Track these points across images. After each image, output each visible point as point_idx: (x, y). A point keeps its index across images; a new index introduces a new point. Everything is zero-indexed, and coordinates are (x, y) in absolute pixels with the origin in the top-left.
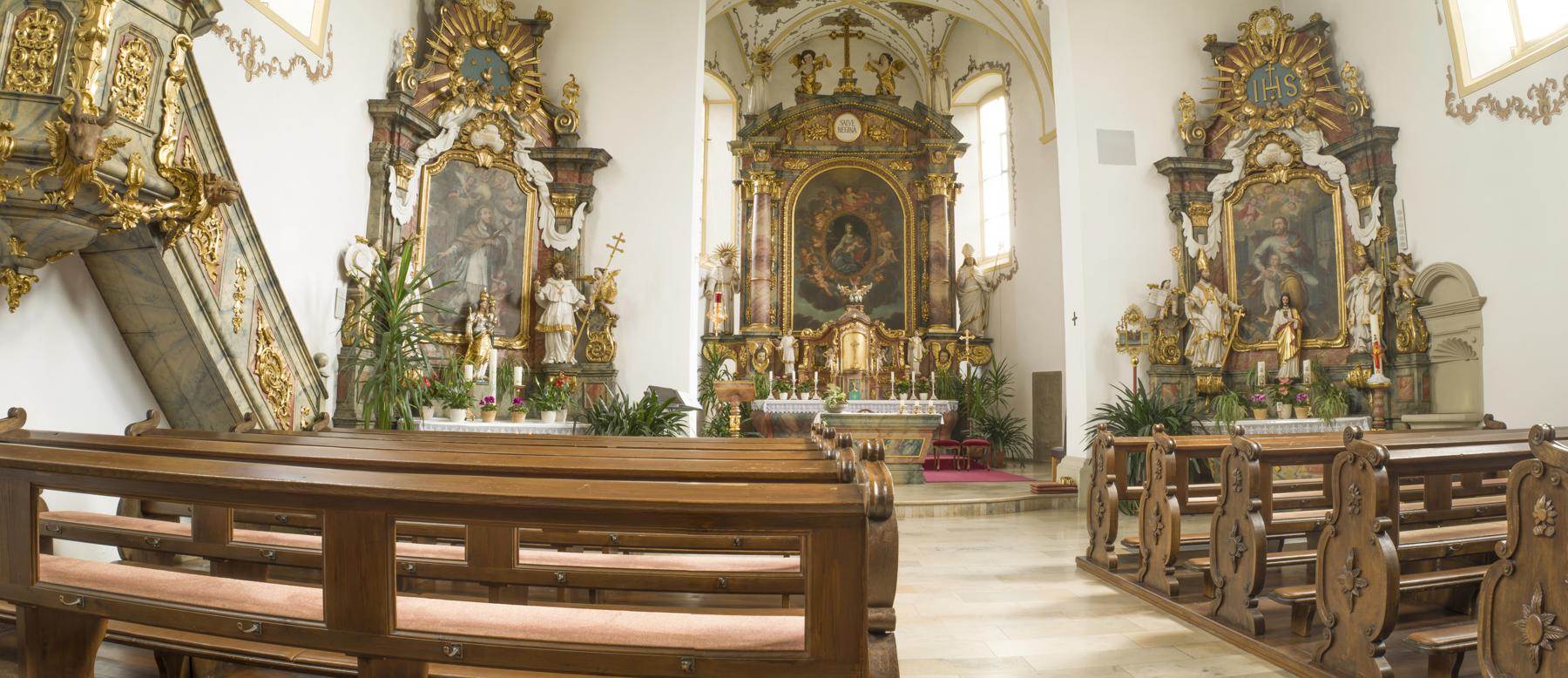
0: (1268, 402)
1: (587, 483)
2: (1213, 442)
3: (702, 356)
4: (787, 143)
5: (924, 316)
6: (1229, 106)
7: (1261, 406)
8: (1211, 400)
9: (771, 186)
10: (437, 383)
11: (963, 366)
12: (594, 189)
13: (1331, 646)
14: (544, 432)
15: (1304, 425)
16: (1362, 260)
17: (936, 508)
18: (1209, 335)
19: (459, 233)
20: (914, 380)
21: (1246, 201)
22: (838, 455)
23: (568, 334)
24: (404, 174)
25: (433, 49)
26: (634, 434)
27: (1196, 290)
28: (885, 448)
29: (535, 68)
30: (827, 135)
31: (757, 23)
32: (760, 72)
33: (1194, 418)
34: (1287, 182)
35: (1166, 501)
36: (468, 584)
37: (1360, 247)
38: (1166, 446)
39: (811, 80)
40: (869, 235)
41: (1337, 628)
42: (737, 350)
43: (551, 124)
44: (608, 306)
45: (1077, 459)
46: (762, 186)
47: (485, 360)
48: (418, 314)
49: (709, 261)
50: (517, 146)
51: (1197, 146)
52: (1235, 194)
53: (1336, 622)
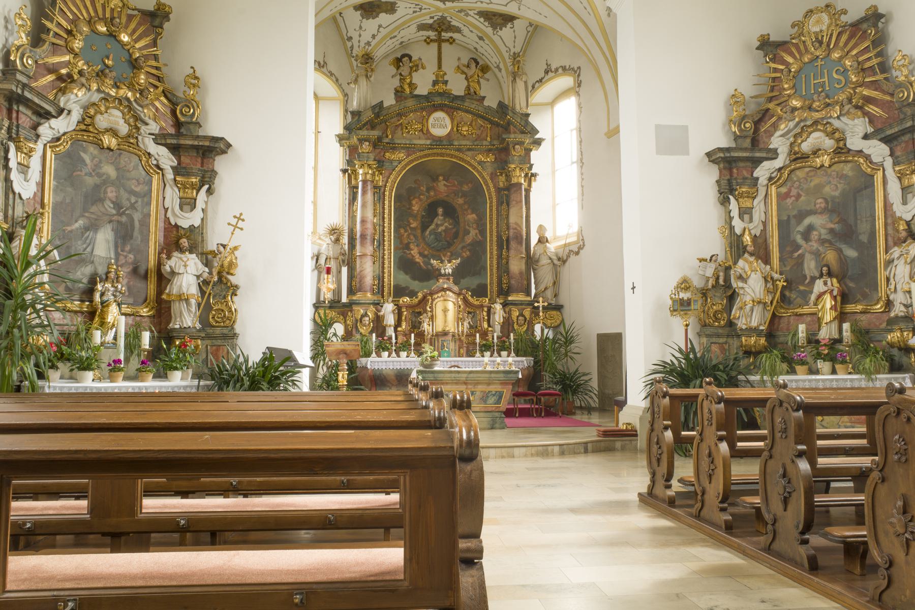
0: (809, 359)
1: (207, 435)
2: (758, 394)
3: (314, 320)
4: (387, 136)
5: (504, 286)
6: (777, 100)
7: (803, 363)
8: (755, 358)
9: (373, 175)
10: (64, 348)
11: (538, 328)
12: (216, 173)
13: (888, 586)
14: (170, 390)
15: (846, 380)
16: (904, 234)
17: (516, 450)
18: (753, 301)
19: (85, 210)
20: (495, 340)
21: (789, 184)
22: (431, 405)
23: (193, 301)
24: (25, 151)
25: (49, 30)
26: (254, 390)
27: (741, 263)
28: (471, 398)
29: (156, 58)
30: (422, 130)
31: (361, 27)
32: (364, 73)
33: (740, 373)
34: (830, 166)
35: (716, 445)
36: (91, 536)
37: (901, 222)
38: (715, 397)
39: (408, 81)
40: (458, 217)
41: (892, 569)
42: (345, 315)
43: (174, 112)
44: (230, 277)
45: (637, 408)
46: (366, 174)
47: (113, 325)
48: (44, 283)
49: (320, 238)
50: (142, 131)
51: (745, 137)
52: (779, 179)
53: (891, 564)
